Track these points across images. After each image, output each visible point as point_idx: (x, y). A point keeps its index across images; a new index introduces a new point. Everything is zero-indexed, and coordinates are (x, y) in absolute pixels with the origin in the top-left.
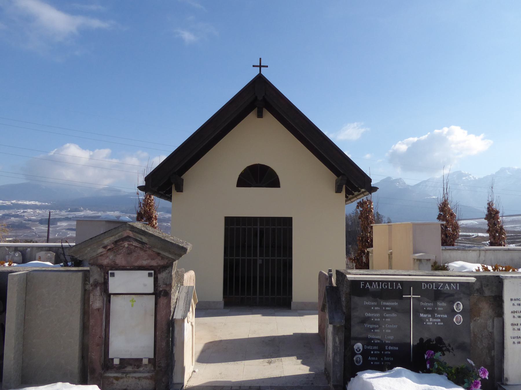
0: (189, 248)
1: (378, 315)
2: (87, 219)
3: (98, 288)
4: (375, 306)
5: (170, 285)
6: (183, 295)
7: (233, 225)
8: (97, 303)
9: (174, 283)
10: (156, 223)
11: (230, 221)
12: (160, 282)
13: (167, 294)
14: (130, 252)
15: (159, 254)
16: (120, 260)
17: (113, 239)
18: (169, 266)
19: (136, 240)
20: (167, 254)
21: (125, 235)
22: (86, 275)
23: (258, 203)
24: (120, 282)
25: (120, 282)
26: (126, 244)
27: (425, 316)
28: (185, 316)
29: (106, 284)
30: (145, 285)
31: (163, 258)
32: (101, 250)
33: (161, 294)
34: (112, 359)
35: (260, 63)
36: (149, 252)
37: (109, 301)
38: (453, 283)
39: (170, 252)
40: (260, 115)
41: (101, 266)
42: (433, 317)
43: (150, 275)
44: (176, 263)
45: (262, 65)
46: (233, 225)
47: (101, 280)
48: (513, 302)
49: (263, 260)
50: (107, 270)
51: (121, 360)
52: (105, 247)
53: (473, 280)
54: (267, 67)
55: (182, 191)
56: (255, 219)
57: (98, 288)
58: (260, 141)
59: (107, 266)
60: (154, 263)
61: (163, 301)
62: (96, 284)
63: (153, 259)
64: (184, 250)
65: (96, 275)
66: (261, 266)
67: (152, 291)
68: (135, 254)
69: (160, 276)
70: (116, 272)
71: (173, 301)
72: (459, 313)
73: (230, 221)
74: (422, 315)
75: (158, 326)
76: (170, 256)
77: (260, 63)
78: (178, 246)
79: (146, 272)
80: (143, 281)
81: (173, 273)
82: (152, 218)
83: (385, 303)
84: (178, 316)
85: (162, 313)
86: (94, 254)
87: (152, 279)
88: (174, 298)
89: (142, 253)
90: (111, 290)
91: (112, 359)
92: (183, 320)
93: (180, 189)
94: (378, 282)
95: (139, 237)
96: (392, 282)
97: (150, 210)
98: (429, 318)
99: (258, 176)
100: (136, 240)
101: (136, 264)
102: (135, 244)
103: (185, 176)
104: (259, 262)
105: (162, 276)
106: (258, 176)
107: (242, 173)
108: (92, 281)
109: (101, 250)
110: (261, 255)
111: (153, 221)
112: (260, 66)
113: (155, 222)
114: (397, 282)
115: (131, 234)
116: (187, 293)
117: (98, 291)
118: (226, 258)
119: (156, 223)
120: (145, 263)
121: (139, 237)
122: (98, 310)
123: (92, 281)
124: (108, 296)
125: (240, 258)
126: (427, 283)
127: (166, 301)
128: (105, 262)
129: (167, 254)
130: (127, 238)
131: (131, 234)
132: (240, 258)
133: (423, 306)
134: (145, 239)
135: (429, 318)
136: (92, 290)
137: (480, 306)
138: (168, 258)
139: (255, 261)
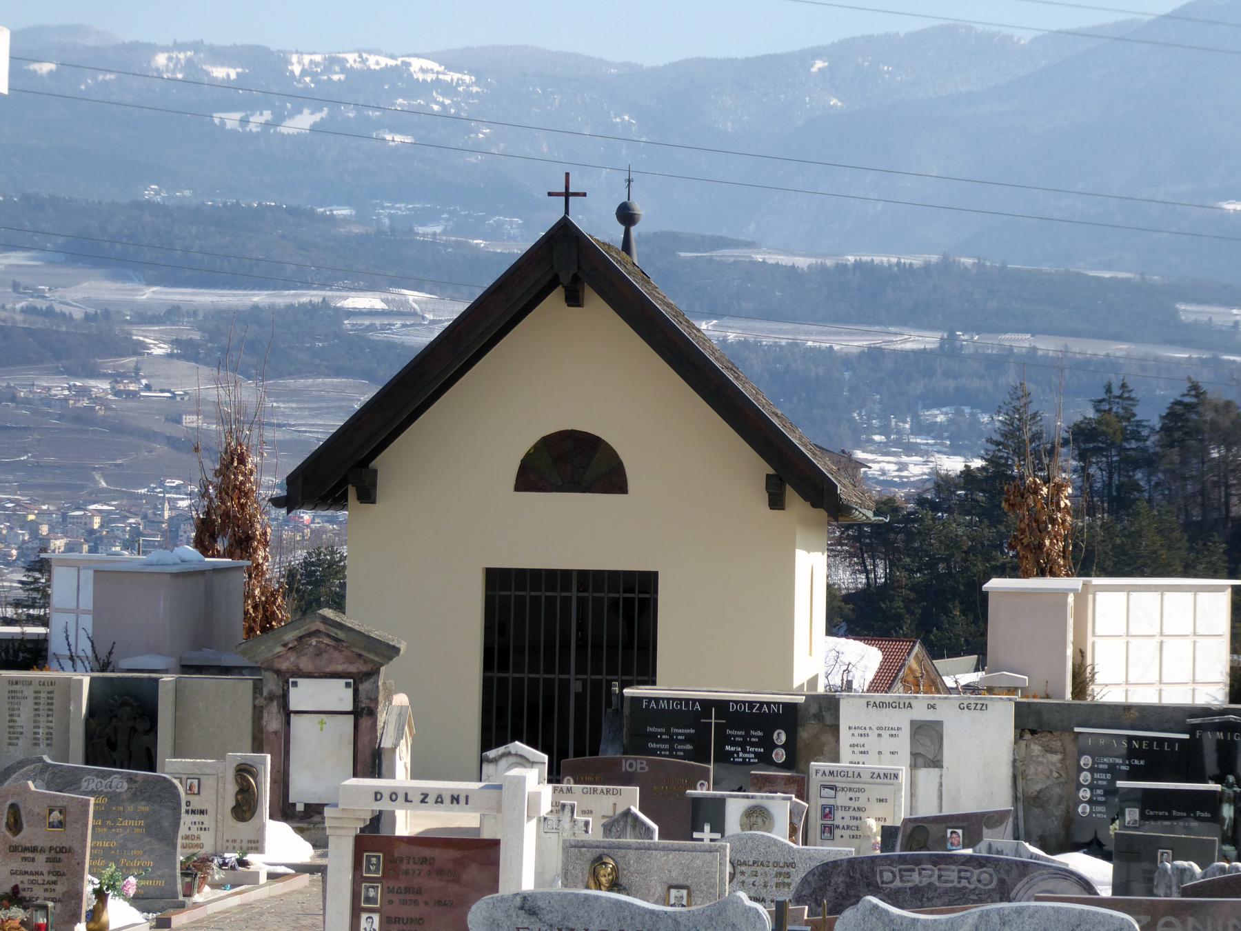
0: (403, 647)
1: (667, 746)
2: (151, 569)
3: (275, 703)
4: (661, 734)
5: (375, 700)
6: (393, 718)
7: (505, 589)
8: (273, 723)
9: (381, 698)
10: (266, 558)
11: (497, 579)
12: (362, 695)
13: (372, 713)
14: (319, 653)
15: (360, 656)
16: (305, 664)
17: (296, 633)
18: (373, 673)
19: (329, 636)
20: (371, 656)
21: (314, 629)
22: (257, 688)
23: (571, 535)
24: (304, 694)
25: (304, 694)
26: (314, 641)
27: (733, 749)
28: (396, 745)
29: (284, 697)
30: (341, 700)
31: (366, 661)
32: (279, 649)
33: (363, 713)
34: (294, 805)
35: (567, 188)
36: (347, 653)
37: (288, 723)
38: (775, 703)
39: (376, 653)
40: (574, 300)
41: (278, 672)
42: (744, 751)
43: (348, 685)
44: (383, 669)
45: (571, 190)
46: (505, 589)
47: (279, 692)
48: (853, 731)
49: (585, 681)
50: (287, 677)
51: (306, 805)
52: (285, 645)
53: (801, 699)
54: (584, 195)
55: (374, 502)
56: (566, 574)
57: (275, 703)
58: (570, 372)
59: (287, 672)
60: (353, 669)
61: (365, 722)
62: (271, 698)
63: (351, 663)
64: (396, 650)
65: (271, 684)
66: (580, 697)
67: (350, 708)
68: (326, 656)
69: (361, 687)
70: (300, 681)
71: (380, 724)
72: (778, 746)
73: (497, 579)
74: (728, 748)
75: (360, 757)
76: (376, 659)
77: (567, 188)
78: (388, 645)
79: (343, 682)
80: (338, 694)
81: (380, 684)
82: (249, 538)
83: (676, 730)
84: (386, 743)
85: (364, 740)
86: (269, 655)
87: (350, 691)
88: (382, 717)
89: (336, 654)
90: (293, 706)
91: (294, 805)
92: (393, 750)
93: (367, 496)
94: (668, 699)
95: (333, 631)
96: (687, 701)
97: (242, 507)
98: (737, 753)
99: (572, 463)
100: (329, 636)
101: (328, 670)
102: (326, 641)
103: (378, 463)
104: (576, 687)
105: (364, 687)
106: (572, 463)
107: (528, 454)
108: (265, 693)
109: (279, 649)
110: (581, 670)
111: (255, 550)
112: (567, 194)
113: (261, 553)
114: (695, 701)
115: (322, 627)
116: (400, 715)
117: (274, 708)
118: (489, 674)
119: (266, 558)
120: (340, 668)
121: (333, 631)
122: (276, 733)
123: (265, 693)
124: (287, 714)
125: (526, 676)
126: (737, 702)
127: (370, 722)
128: (284, 666)
129: (371, 656)
130: (317, 633)
131: (322, 627)
132: (526, 676)
133: (731, 736)
134: (341, 635)
135: (737, 753)
136: (267, 705)
137: (823, 739)
138: (372, 661)
139: (565, 685)
